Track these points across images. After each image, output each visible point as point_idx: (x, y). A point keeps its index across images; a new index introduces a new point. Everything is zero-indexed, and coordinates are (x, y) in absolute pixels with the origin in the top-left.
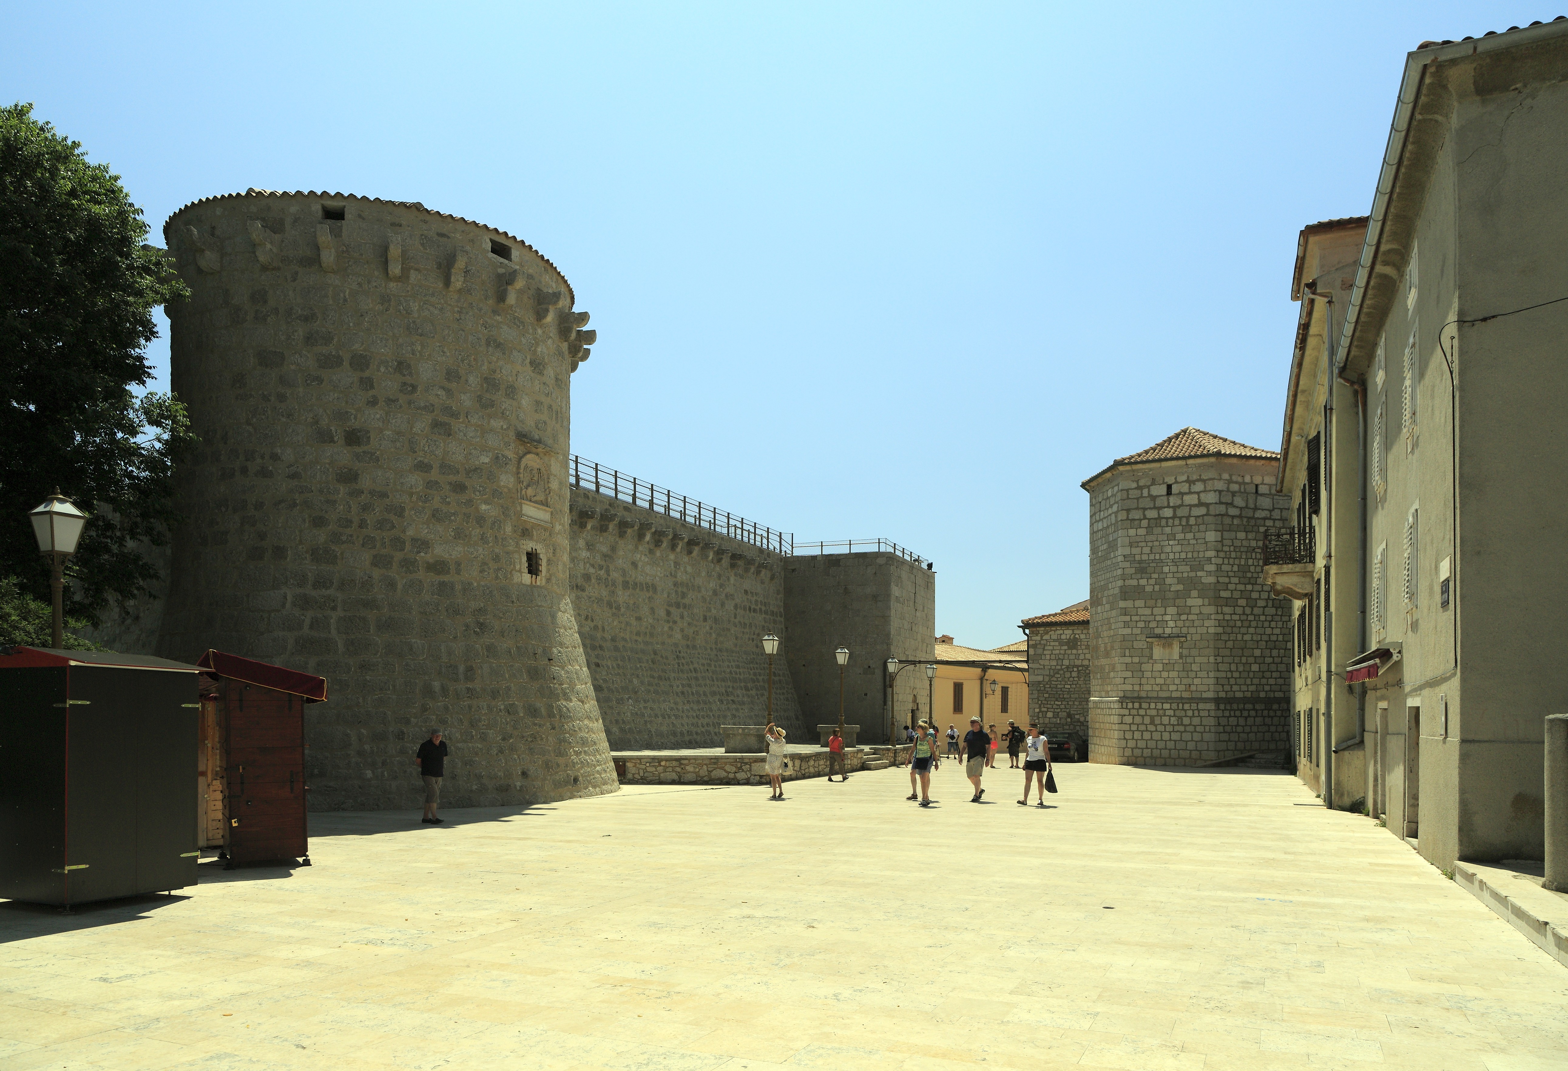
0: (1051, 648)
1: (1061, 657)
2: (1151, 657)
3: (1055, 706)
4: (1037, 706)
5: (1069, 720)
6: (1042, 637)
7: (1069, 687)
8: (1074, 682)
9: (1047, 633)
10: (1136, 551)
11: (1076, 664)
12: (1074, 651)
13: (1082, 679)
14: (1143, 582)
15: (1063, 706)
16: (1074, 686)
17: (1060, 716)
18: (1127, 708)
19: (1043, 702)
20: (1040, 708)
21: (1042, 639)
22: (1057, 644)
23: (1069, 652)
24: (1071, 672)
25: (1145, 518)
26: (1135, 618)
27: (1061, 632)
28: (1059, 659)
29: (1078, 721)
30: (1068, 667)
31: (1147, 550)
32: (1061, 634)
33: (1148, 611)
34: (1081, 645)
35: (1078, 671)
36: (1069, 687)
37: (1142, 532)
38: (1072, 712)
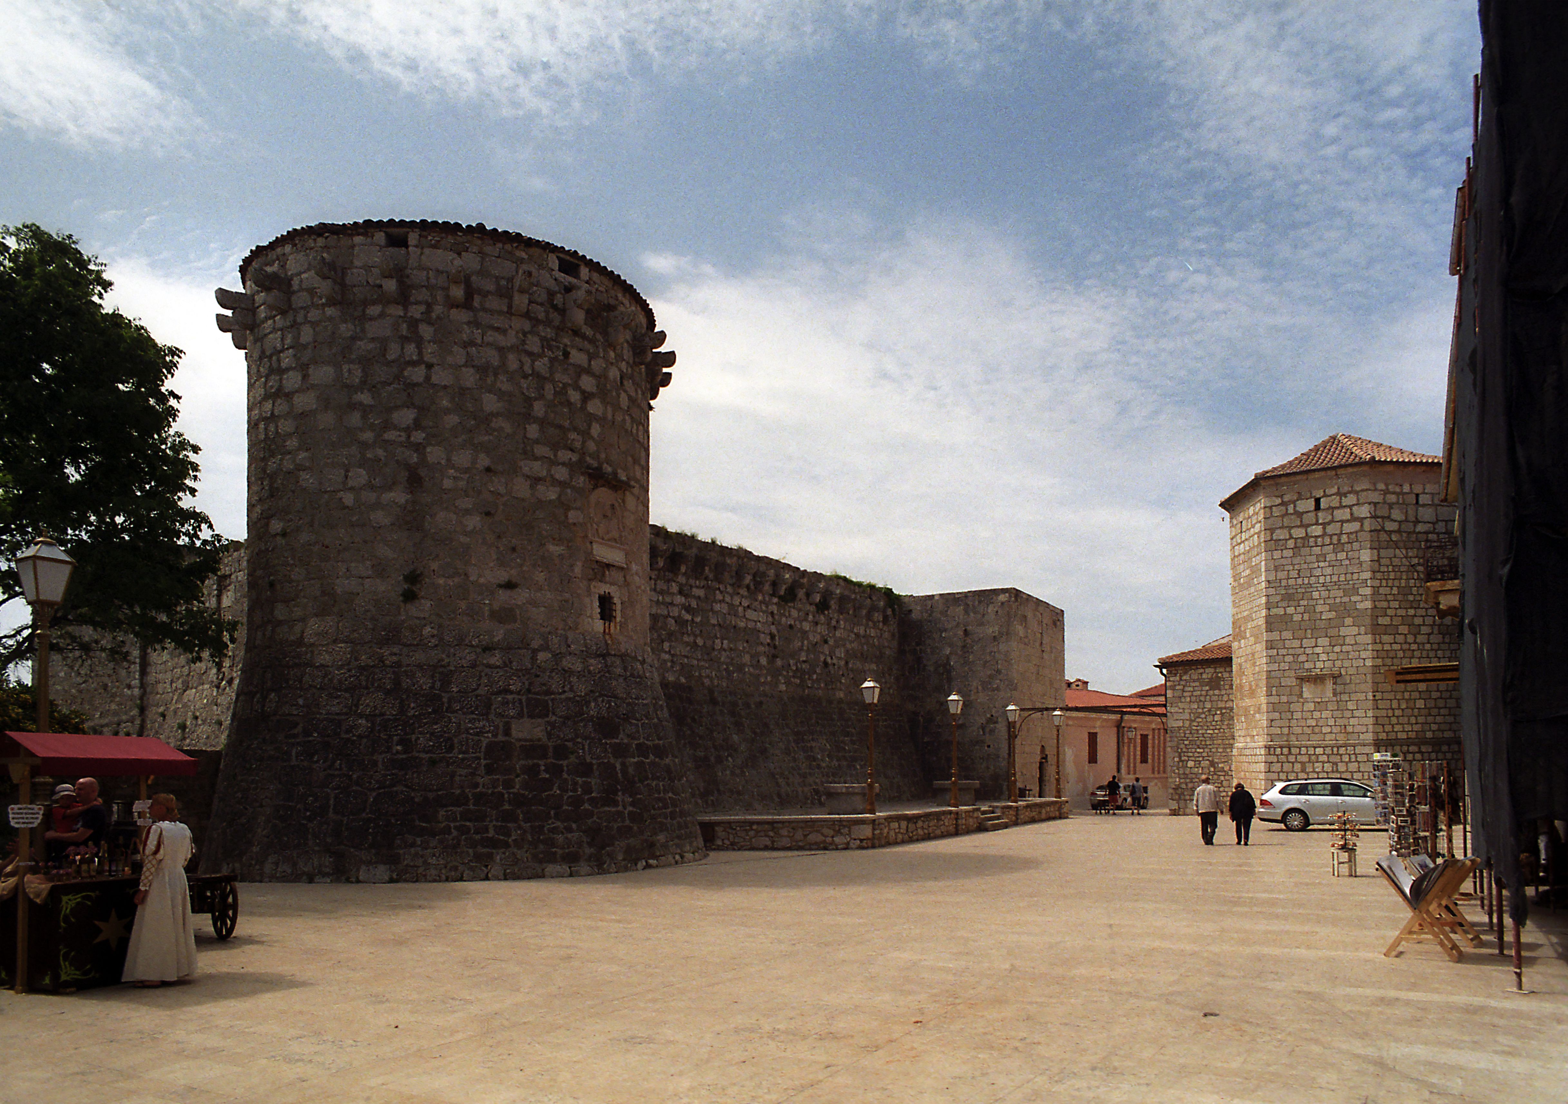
0: (1191, 689)
1: (1202, 699)
2: (1301, 695)
3: (1196, 755)
4: (1177, 754)
5: (1212, 769)
6: (1181, 676)
7: (1211, 732)
8: (1218, 727)
9: (1185, 673)
10: (1282, 575)
11: (1219, 706)
12: (1217, 692)
13: (1226, 723)
14: (1290, 610)
15: (1205, 754)
16: (1216, 731)
17: (1202, 765)
18: (1274, 754)
19: (1184, 750)
20: (1180, 757)
21: (1181, 679)
22: (1197, 684)
23: (1211, 692)
24: (1213, 715)
25: (1291, 537)
26: (1282, 652)
27: (1201, 671)
28: (1201, 701)
29: (1222, 770)
30: (1209, 711)
31: (1294, 574)
32: (1201, 674)
33: (1296, 643)
34: (1224, 685)
35: (1222, 714)
36: (1211, 732)
37: (1288, 553)
38: (1216, 760)
